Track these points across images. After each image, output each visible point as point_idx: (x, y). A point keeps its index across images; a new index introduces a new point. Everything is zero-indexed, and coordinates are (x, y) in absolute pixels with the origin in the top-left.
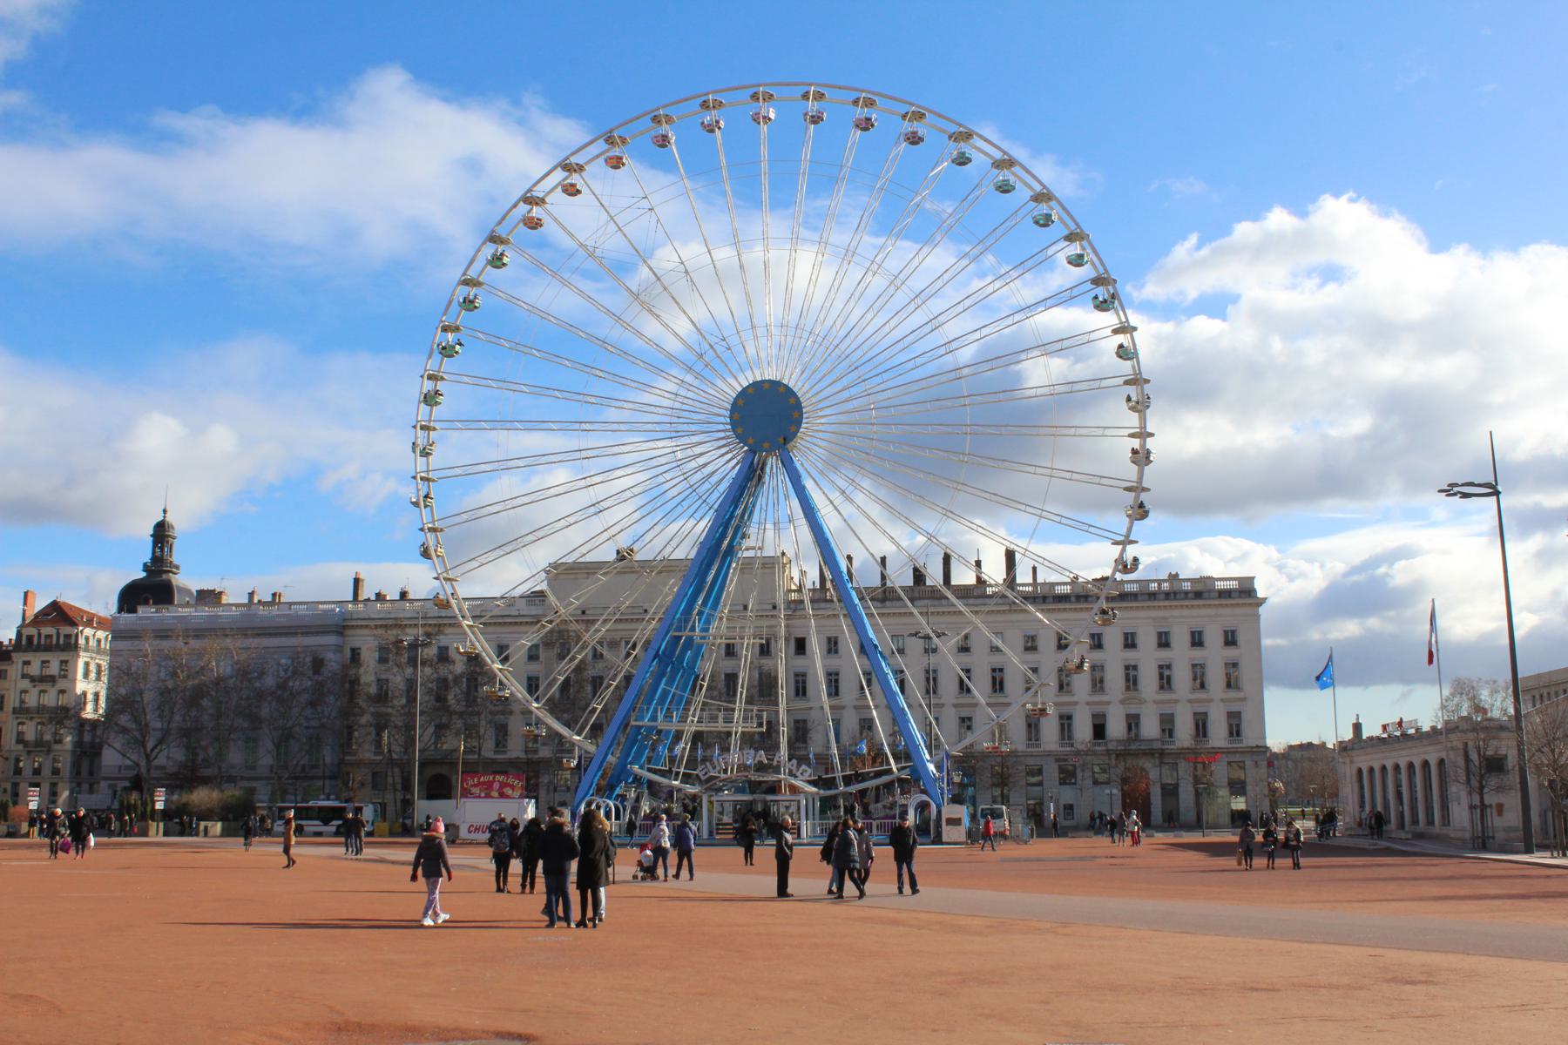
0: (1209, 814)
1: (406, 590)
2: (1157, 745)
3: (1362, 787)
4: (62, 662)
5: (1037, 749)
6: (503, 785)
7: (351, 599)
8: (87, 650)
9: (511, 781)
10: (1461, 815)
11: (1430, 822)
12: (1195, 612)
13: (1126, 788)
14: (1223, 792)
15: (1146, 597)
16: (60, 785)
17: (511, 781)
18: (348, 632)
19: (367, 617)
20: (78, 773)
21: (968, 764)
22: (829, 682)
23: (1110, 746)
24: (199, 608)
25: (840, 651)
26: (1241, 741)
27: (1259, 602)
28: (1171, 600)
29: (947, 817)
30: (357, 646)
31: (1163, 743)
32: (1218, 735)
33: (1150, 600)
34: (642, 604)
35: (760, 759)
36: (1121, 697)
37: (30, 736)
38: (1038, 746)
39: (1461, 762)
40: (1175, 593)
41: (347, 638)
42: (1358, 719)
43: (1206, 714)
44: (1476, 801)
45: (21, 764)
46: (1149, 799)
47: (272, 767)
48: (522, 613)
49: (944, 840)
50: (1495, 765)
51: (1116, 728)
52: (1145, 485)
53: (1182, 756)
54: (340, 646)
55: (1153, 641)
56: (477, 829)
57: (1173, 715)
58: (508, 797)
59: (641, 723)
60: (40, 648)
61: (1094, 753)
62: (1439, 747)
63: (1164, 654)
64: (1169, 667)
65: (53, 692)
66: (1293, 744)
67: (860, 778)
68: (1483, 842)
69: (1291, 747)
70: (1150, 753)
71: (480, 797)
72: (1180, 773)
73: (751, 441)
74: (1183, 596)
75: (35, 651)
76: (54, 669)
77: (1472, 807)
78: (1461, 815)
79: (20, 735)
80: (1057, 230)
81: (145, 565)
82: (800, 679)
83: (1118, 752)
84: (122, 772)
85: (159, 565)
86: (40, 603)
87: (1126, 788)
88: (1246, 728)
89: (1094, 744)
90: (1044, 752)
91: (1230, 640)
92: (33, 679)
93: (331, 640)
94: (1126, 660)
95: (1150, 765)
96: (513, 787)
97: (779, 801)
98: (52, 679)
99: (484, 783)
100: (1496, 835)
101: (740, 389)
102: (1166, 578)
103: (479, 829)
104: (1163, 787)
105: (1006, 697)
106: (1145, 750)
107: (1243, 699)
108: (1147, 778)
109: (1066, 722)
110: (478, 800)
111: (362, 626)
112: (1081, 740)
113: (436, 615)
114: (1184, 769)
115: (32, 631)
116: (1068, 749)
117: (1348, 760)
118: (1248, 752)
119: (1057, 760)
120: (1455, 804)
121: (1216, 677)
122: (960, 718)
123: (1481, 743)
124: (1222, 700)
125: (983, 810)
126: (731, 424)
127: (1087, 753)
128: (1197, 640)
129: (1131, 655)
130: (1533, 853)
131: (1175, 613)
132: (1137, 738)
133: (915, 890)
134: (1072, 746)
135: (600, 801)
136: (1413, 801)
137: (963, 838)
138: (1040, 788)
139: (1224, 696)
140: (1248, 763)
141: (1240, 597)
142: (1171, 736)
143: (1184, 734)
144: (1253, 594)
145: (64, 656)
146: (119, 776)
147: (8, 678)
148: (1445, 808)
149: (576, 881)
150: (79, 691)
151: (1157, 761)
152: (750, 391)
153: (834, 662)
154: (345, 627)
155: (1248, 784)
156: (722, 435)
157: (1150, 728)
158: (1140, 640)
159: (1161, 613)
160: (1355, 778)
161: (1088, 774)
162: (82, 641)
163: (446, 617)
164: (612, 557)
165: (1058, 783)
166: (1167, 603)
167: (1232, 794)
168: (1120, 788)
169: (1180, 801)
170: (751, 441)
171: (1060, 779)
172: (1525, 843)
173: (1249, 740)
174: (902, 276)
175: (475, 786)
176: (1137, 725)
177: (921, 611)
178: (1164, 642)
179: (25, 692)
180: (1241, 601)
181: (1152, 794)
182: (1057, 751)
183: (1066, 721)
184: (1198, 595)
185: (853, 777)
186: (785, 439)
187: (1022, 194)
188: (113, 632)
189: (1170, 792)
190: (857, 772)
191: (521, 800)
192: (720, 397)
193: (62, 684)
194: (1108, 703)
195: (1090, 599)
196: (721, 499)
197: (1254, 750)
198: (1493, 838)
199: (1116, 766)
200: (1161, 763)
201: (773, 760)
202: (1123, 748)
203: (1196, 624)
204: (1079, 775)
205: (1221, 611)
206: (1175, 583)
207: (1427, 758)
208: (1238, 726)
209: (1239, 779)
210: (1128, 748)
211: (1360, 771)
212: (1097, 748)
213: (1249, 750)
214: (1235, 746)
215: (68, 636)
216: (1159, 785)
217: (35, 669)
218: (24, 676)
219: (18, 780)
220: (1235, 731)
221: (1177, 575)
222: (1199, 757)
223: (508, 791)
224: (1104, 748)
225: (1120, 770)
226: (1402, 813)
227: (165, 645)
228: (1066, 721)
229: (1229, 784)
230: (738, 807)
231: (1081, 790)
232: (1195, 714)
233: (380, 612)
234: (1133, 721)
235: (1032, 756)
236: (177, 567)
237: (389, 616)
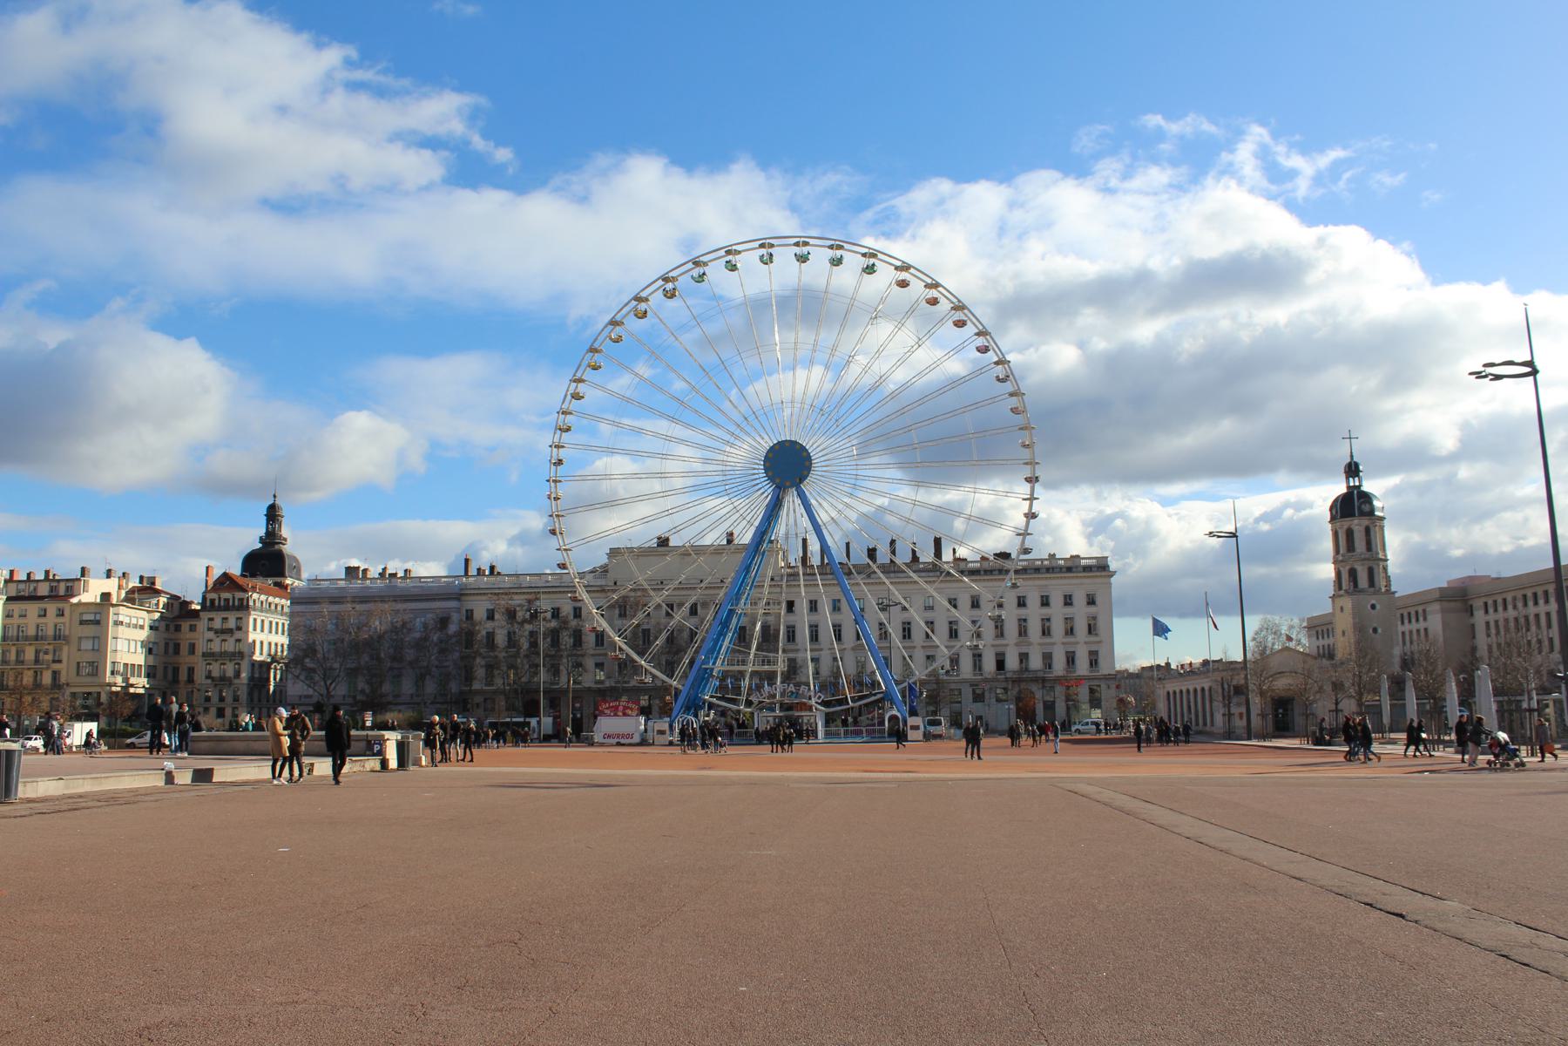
2: (1040, 674)
4: (237, 619)
6: (625, 708)
8: (255, 610)
9: (630, 705)
11: (1205, 724)
13: (1020, 704)
15: (1033, 571)
16: (240, 709)
18: (463, 598)
20: (252, 700)
22: (811, 632)
23: (1008, 676)
24: (353, 581)
26: (1098, 671)
30: (471, 608)
31: (1045, 673)
32: (1082, 667)
33: (1035, 573)
36: (1015, 641)
37: (216, 674)
39: (1220, 690)
40: (1053, 569)
43: (1074, 652)
45: (239, 693)
47: (344, 696)
48: (591, 584)
51: (1012, 663)
55: (1038, 601)
58: (629, 716)
59: (707, 667)
60: (219, 609)
61: (998, 680)
64: (1048, 620)
65: (231, 641)
68: (1229, 734)
70: (1035, 680)
71: (610, 716)
75: (218, 611)
76: (232, 624)
77: (1224, 715)
79: (209, 677)
80: (970, 329)
81: (261, 538)
82: (791, 629)
85: (271, 538)
86: (217, 573)
87: (1020, 704)
89: (997, 675)
91: (1091, 601)
92: (216, 632)
93: (453, 604)
94: (1018, 615)
95: (1036, 688)
96: (632, 709)
98: (230, 631)
99: (613, 707)
104: (1045, 703)
107: (1100, 642)
109: (977, 659)
114: (1059, 691)
115: (214, 596)
121: (1081, 627)
124: (1086, 643)
127: (993, 680)
128: (1068, 601)
129: (1022, 612)
131: (1054, 582)
132: (1027, 670)
133: (1318, 647)
134: (981, 675)
137: (921, 738)
138: (959, 705)
139: (1087, 640)
142: (1050, 667)
145: (239, 614)
147: (198, 630)
148: (1212, 715)
149: (1561, 660)
150: (250, 640)
151: (1040, 686)
153: (815, 618)
156: (768, 486)
157: (1036, 663)
158: (1028, 602)
160: (1166, 698)
161: (993, 695)
162: (251, 603)
166: (1048, 575)
170: (778, 481)
173: (1104, 669)
178: (1045, 602)
179: (211, 641)
180: (1098, 574)
183: (977, 657)
184: (1069, 569)
187: (944, 305)
188: (291, 599)
189: (1050, 707)
193: (238, 635)
195: (994, 573)
200: (1044, 687)
203: (1068, 591)
206: (1053, 561)
208: (1096, 660)
211: (1168, 693)
215: (241, 600)
217: (217, 624)
218: (210, 629)
219: (223, 706)
220: (1094, 662)
221: (1054, 555)
224: (1003, 677)
225: (1015, 692)
227: (336, 608)
228: (977, 657)
230: (777, 720)
232: (1067, 652)
233: (487, 583)
234: (1024, 657)
236: (285, 539)
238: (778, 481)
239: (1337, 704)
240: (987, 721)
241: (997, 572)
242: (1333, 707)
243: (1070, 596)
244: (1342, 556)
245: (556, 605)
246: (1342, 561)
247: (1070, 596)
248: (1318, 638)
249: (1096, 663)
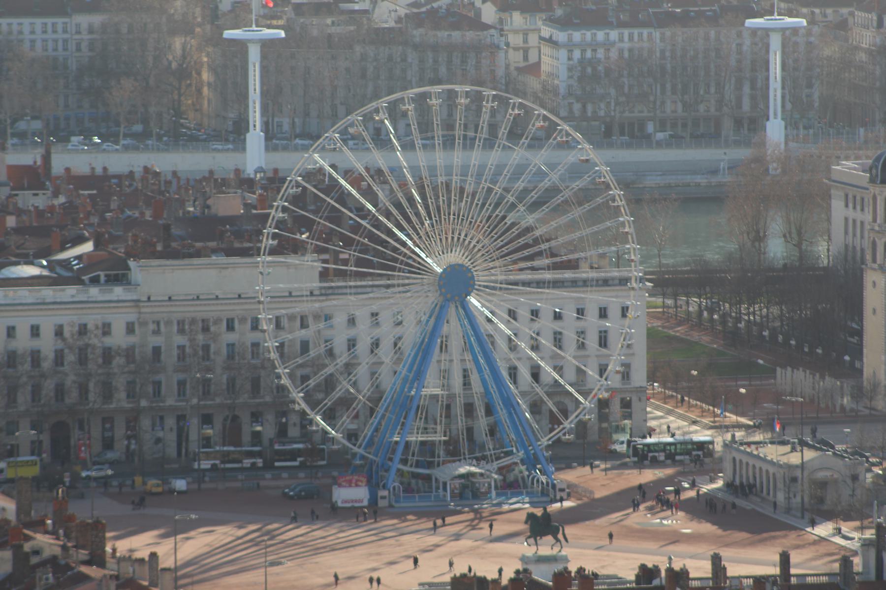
26: (630, 384)
44: (787, 496)
48: (121, 298)
50: (794, 480)
96: (362, 481)
107: (633, 354)
125: (277, 122)
128: (603, 313)
195: (532, 285)
203: (34, 321)
209: (478, 489)
223: (360, 484)
238: (443, 290)
239: (853, 491)
240: (380, 382)
241: (535, 285)
242: (851, 493)
243: (605, 309)
244: (879, 226)
245: (83, 321)
246: (878, 232)
247: (605, 309)
248: (847, 206)
249: (628, 377)
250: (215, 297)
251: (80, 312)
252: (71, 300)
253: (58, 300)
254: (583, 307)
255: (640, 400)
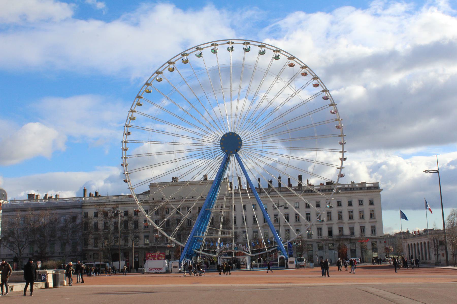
0: (366, 259)
1: (97, 191)
2: (349, 237)
3: (409, 249)
5: (311, 239)
6: (159, 256)
7: (83, 197)
10: (433, 257)
11: (426, 259)
12: (360, 194)
13: (340, 251)
14: (370, 251)
17: (161, 255)
18: (83, 207)
19: (90, 202)
21: (290, 246)
23: (334, 238)
25: (246, 210)
26: (376, 235)
27: (380, 190)
28: (352, 190)
29: (290, 261)
31: (351, 236)
33: (345, 191)
34: (181, 196)
35: (244, 248)
38: (311, 238)
40: (353, 188)
41: (83, 209)
42: (408, 229)
46: (347, 254)
47: (28, 254)
49: (289, 268)
51: (336, 232)
52: (343, 167)
53: (357, 240)
54: (81, 212)
55: (347, 203)
56: (151, 269)
57: (354, 227)
58: (160, 259)
62: (427, 238)
63: (350, 208)
66: (397, 232)
67: (261, 250)
68: (438, 264)
69: (396, 234)
70: (346, 240)
71: (152, 260)
72: (356, 246)
73: (226, 151)
74: (356, 189)
77: (435, 255)
78: (433, 257)
83: (337, 239)
84: (29, 255)
87: (340, 251)
88: (377, 231)
90: (313, 240)
91: (371, 203)
93: (79, 210)
96: (162, 257)
97: (240, 258)
99: (153, 256)
100: (441, 262)
101: (223, 135)
102: (351, 183)
103: (152, 269)
104: (351, 250)
105: (300, 223)
106: (345, 239)
107: (376, 222)
108: (346, 248)
110: (151, 261)
111: (88, 205)
112: (325, 236)
113: (113, 201)
114: (358, 244)
116: (321, 239)
117: (405, 242)
118: (378, 238)
119: (317, 243)
120: (432, 254)
122: (285, 230)
123: (437, 237)
126: (220, 146)
127: (327, 240)
128: (361, 203)
130: (448, 266)
131: (354, 194)
132: (342, 235)
134: (322, 238)
135: (186, 259)
136: (422, 253)
137: (295, 267)
138: (311, 252)
140: (378, 242)
141: (374, 189)
142: (353, 234)
143: (357, 233)
144: (378, 188)
146: (7, 257)
148: (429, 255)
151: (349, 242)
152: (226, 136)
154: (83, 206)
155: (378, 248)
157: (346, 232)
159: (349, 195)
160: (407, 246)
161: (327, 247)
163: (116, 202)
164: (171, 180)
165: (317, 250)
167: (373, 252)
168: (337, 251)
169: (357, 255)
170: (226, 151)
171: (318, 249)
172: (447, 264)
173: (378, 234)
174: (272, 101)
175: (150, 256)
176: (342, 230)
177: (271, 196)
178: (350, 204)
181: (348, 252)
182: (317, 240)
184: (361, 189)
185: (259, 250)
186: (237, 150)
190: (260, 249)
191: (164, 260)
192: (215, 139)
194: (333, 224)
195: (326, 191)
196: (218, 170)
197: (380, 238)
198: (440, 262)
199: (336, 244)
200: (350, 243)
201: (238, 246)
202: (338, 238)
203: (361, 198)
204: (324, 247)
205: (368, 194)
206: (354, 185)
207: (425, 241)
210: (340, 238)
211: (409, 245)
212: (330, 238)
213: (378, 238)
214: (374, 236)
216: (350, 249)
220: (373, 231)
221: (354, 182)
222: (363, 240)
223: (160, 258)
226: (420, 257)
229: (372, 249)
231: (325, 252)
233: (94, 200)
234: (341, 229)
235: (309, 241)
237: (97, 202)
241: (328, 191)
250: (271, 193)
251: (125, 205)
252: (121, 200)
253: (116, 201)
254: (362, 200)
255: (381, 242)
